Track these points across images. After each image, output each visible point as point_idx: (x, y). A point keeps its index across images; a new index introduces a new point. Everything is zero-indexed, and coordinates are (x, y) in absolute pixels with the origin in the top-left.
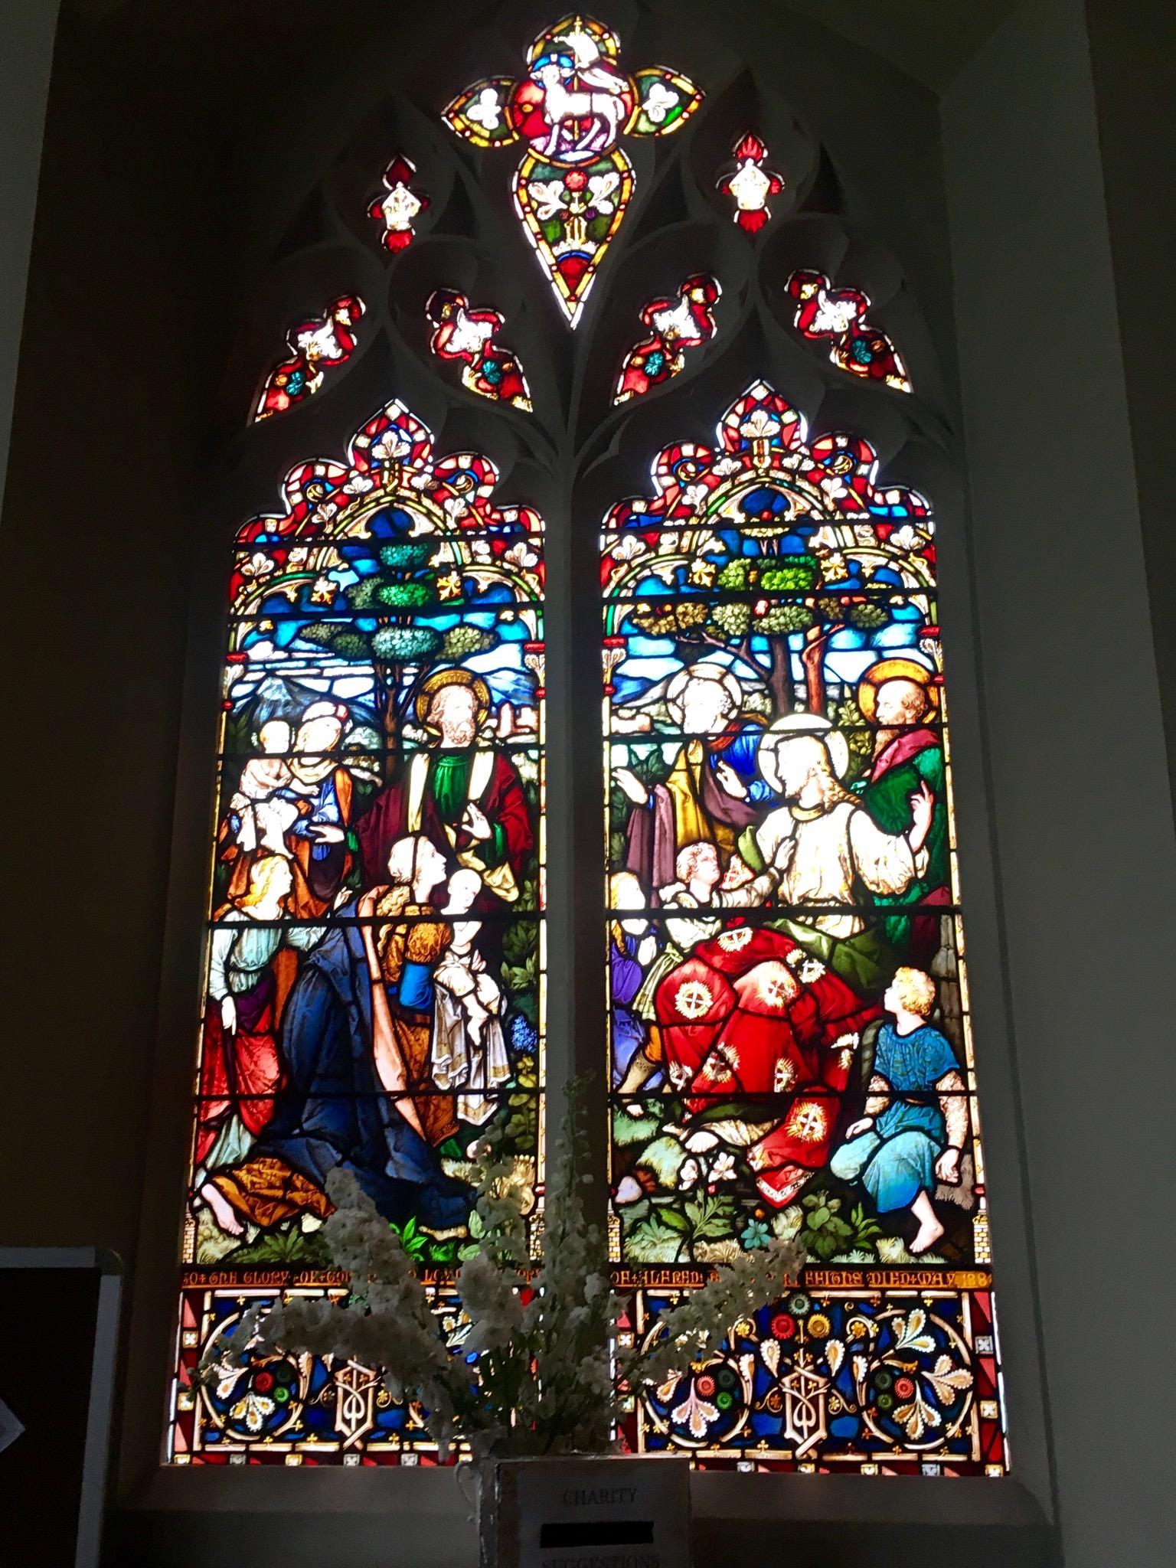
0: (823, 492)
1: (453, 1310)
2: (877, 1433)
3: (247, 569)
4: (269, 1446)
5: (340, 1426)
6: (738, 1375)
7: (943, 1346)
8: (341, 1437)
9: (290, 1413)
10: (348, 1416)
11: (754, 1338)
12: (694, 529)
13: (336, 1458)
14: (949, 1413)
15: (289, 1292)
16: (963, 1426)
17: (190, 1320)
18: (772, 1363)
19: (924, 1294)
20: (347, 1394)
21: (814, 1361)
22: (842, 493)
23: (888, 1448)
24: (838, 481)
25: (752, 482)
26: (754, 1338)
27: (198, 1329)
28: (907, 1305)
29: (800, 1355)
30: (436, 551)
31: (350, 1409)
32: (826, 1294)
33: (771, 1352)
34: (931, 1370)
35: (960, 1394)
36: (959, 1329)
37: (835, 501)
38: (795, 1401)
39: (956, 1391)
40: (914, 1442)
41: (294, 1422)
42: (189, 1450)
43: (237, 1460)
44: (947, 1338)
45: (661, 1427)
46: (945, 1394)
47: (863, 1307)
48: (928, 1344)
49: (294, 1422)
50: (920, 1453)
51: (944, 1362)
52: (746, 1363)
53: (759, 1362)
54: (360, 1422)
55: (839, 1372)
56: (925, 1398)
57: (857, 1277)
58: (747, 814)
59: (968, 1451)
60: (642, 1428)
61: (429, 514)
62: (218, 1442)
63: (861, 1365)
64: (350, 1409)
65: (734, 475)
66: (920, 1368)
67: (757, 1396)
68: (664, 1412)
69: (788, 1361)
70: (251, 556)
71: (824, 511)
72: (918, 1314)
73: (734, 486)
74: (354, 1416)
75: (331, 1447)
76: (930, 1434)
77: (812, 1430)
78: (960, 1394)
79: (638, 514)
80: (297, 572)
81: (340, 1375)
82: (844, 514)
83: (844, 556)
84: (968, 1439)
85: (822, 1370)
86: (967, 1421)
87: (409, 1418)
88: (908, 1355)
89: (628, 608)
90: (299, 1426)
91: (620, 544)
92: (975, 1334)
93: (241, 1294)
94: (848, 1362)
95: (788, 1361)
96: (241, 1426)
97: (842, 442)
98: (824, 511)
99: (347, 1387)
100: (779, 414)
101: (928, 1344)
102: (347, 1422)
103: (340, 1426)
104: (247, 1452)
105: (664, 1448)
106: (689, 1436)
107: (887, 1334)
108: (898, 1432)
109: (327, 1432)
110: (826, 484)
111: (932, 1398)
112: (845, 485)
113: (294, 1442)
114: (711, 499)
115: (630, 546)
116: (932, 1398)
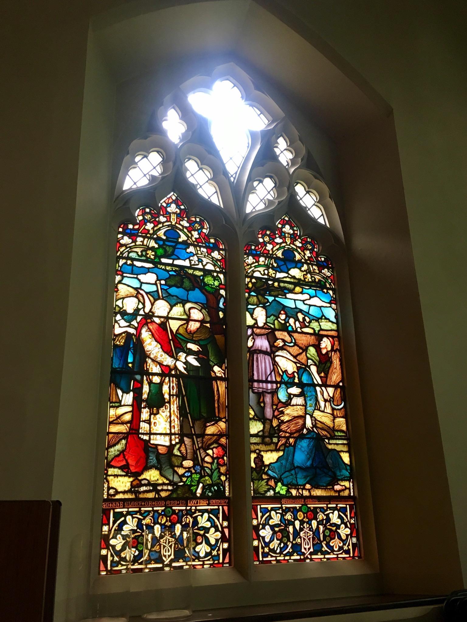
0: (192, 235)
1: (200, 514)
2: (326, 549)
3: (122, 242)
4: (136, 566)
5: (303, 550)
6: (289, 532)
7: (343, 522)
8: (304, 554)
9: (288, 546)
10: (165, 554)
11: (293, 520)
12: (148, 238)
13: (162, 569)
14: (213, 547)
15: (142, 509)
16: (348, 546)
17: (254, 516)
18: (298, 527)
19: (283, 506)
20: (164, 547)
21: (171, 534)
22: (198, 236)
23: (329, 554)
24: (196, 233)
25: (168, 226)
26: (293, 520)
27: (257, 518)
28: (203, 512)
29: (305, 525)
30: (189, 248)
31: (166, 552)
32: (312, 506)
33: (297, 523)
34: (339, 529)
35: (217, 541)
36: (346, 516)
37: (195, 238)
38: (164, 547)
39: (346, 535)
40: (336, 551)
41: (289, 549)
42: (106, 570)
43: (274, 563)
44: (344, 519)
45: (266, 550)
46: (213, 542)
47: (322, 510)
48: (208, 525)
49: (289, 549)
50: (337, 555)
51: (212, 530)
52: (291, 529)
53: (294, 528)
54: (309, 549)
55: (315, 530)
56: (338, 538)
57: (121, 503)
58: (267, 349)
59: (349, 553)
60: (261, 551)
61: (299, 254)
62: (117, 566)
63: (321, 528)
64: (166, 552)
65: (281, 244)
66: (205, 533)
67: (152, 546)
68: (118, 554)
69: (163, 534)
70: (248, 257)
71: (305, 260)
72: (336, 512)
73: (163, 226)
74: (307, 547)
75: (160, 565)
76: (207, 554)
77: (169, 556)
78: (347, 535)
79: (130, 229)
80: (140, 245)
81: (162, 540)
82: (198, 243)
83: (198, 257)
84: (349, 549)
85: (311, 529)
86: (219, 550)
87: (322, 547)
88: (204, 528)
89: (124, 261)
90: (291, 550)
91: (248, 259)
92: (223, 520)
93: (269, 507)
94: (318, 527)
95: (163, 534)
96: (124, 559)
97: (198, 220)
98: (305, 260)
99: (164, 544)
100: (179, 206)
101: (208, 525)
102: (305, 549)
103: (303, 550)
104: (276, 560)
105: (267, 557)
106: (275, 553)
107: (328, 519)
108: (197, 555)
109: (159, 560)
110: (193, 232)
111: (208, 543)
112: (310, 253)
113: (146, 564)
114: (274, 249)
115: (126, 240)
116: (208, 543)
